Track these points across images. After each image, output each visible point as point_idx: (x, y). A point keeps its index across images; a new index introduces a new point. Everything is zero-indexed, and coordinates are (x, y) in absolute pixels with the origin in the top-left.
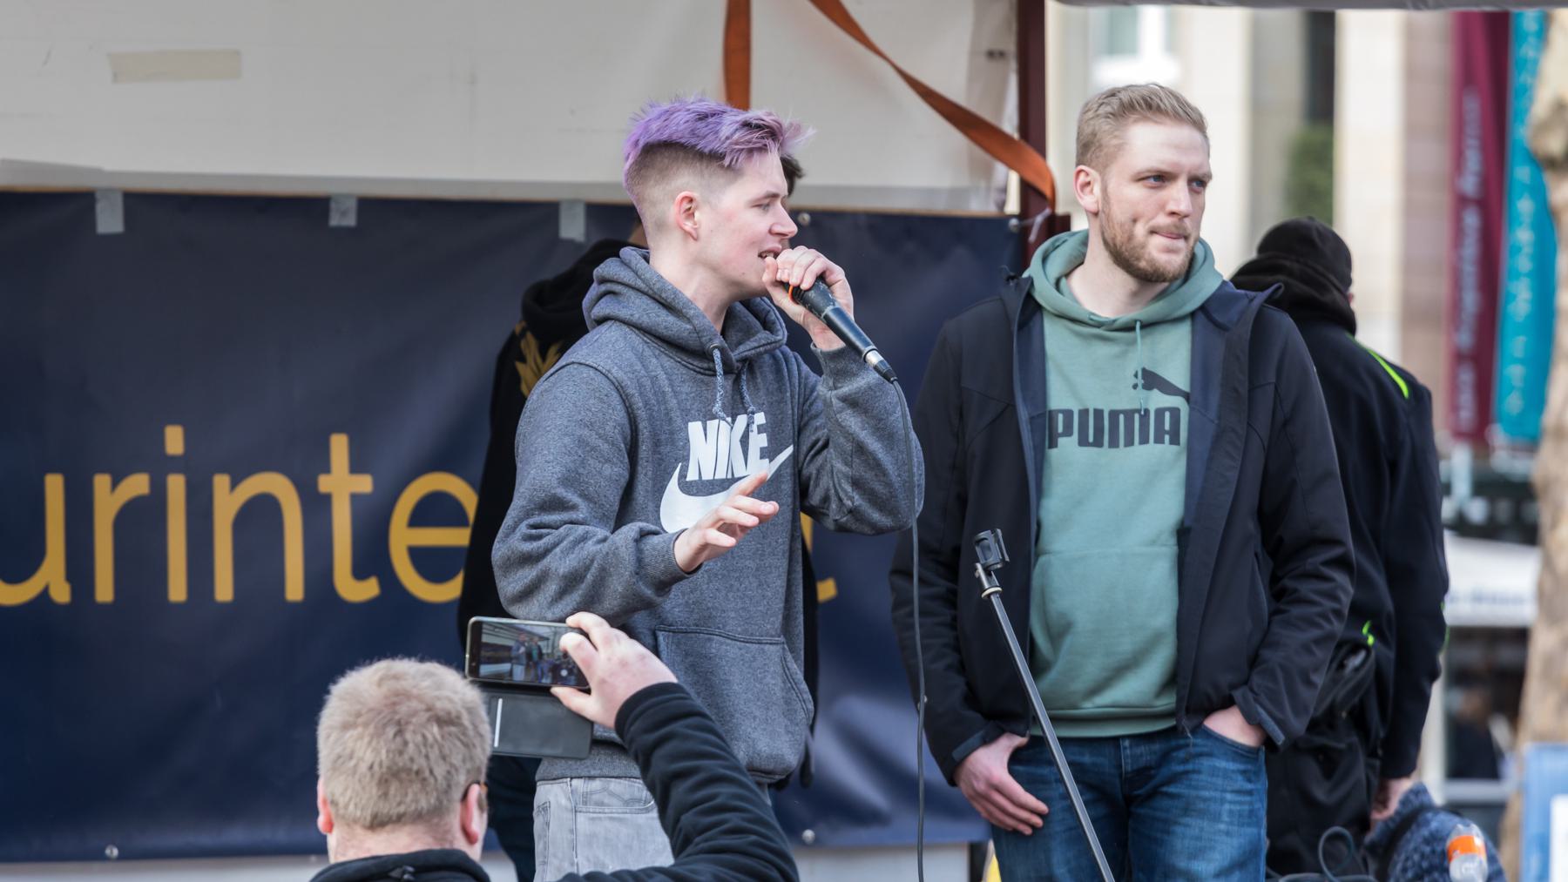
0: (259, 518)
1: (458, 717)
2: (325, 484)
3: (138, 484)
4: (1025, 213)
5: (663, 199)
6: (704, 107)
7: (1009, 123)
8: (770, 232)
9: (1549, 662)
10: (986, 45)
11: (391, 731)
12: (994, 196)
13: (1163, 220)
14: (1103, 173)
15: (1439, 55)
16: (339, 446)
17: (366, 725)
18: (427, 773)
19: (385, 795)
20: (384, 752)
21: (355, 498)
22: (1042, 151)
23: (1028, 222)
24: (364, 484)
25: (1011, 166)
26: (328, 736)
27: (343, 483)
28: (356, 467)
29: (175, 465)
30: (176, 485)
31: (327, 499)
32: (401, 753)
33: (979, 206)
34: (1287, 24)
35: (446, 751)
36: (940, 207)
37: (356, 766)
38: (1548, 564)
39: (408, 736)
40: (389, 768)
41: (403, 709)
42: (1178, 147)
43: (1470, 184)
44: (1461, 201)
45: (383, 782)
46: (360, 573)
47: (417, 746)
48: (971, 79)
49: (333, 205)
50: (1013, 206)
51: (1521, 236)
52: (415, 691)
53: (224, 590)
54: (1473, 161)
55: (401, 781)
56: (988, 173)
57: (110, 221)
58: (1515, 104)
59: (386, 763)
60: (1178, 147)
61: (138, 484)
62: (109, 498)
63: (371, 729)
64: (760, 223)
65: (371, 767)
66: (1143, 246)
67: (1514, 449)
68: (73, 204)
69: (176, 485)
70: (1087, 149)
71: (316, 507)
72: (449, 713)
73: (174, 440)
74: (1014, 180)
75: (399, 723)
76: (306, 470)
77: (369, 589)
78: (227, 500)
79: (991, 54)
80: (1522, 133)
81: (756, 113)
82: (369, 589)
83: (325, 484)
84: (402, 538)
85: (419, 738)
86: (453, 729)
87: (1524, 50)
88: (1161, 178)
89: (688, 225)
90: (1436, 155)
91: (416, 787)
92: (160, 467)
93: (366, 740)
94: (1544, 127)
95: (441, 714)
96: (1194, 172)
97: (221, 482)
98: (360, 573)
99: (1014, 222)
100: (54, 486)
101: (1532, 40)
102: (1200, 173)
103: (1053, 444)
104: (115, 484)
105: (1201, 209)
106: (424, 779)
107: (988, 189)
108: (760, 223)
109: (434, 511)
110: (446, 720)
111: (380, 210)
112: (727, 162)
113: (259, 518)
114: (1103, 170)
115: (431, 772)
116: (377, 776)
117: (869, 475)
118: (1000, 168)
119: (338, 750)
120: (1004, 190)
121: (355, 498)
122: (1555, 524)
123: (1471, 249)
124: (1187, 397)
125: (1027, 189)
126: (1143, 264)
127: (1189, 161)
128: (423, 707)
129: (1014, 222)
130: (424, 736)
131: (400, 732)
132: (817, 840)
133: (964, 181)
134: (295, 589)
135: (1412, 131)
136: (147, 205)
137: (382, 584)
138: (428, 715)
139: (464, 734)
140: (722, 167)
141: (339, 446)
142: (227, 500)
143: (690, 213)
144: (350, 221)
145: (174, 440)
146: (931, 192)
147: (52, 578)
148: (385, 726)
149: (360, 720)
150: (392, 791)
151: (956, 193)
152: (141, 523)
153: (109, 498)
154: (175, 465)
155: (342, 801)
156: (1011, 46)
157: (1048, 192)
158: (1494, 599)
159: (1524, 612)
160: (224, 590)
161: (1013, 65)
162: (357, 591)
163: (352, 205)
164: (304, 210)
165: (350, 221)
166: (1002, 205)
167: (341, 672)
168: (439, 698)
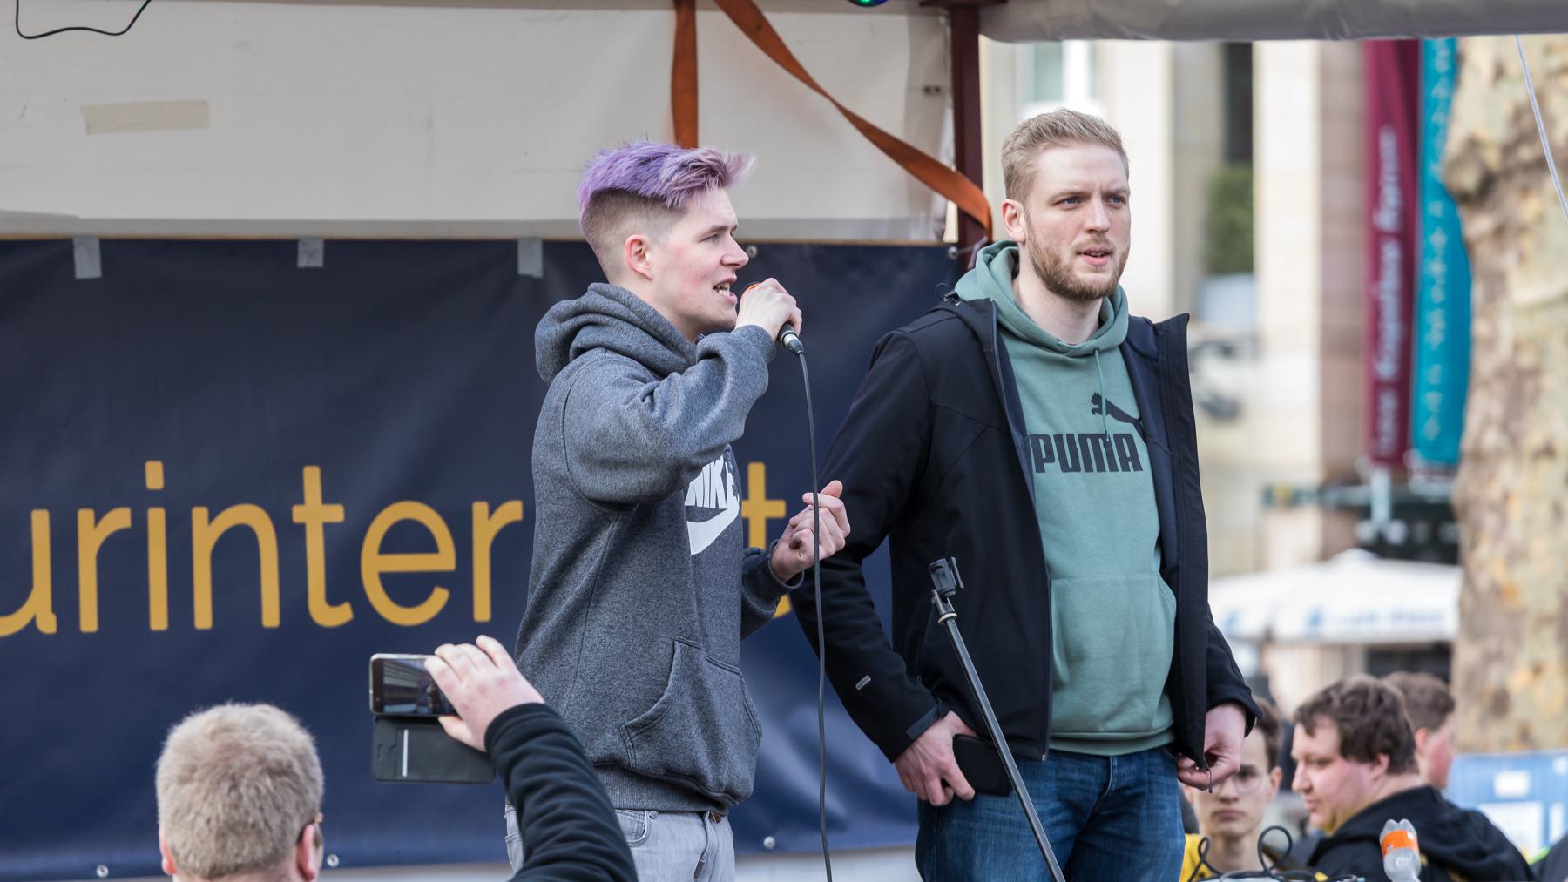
0: (236, 551)
1: (290, 766)
2: (299, 514)
3: (120, 518)
4: (963, 241)
5: (617, 243)
6: (646, 151)
7: (946, 155)
8: (722, 263)
9: (1471, 676)
10: (921, 82)
11: (226, 786)
12: (933, 226)
13: (1083, 239)
14: (1024, 202)
15: (1352, 96)
16: (312, 477)
17: (201, 780)
18: (262, 825)
19: (224, 847)
20: (220, 807)
21: (328, 528)
22: (978, 181)
23: (967, 250)
24: (336, 513)
25: (948, 197)
26: (166, 788)
27: (316, 513)
28: (328, 498)
29: (156, 498)
30: (157, 519)
31: (301, 528)
32: (236, 807)
33: (919, 235)
34: (1204, 56)
35: (280, 801)
36: (882, 237)
37: (193, 821)
38: (1468, 582)
39: (242, 789)
40: (226, 822)
41: (236, 764)
42: (1088, 167)
43: (1387, 219)
44: (1377, 238)
45: (221, 836)
46: (333, 599)
47: (251, 800)
48: (908, 115)
49: (301, 247)
50: (951, 235)
51: (1434, 268)
52: (247, 745)
53: (203, 618)
54: (1391, 196)
55: (237, 834)
56: (927, 204)
57: (87, 267)
58: (1428, 142)
59: (222, 817)
60: (1088, 167)
61: (120, 518)
62: (92, 533)
63: (207, 784)
64: (709, 256)
65: (208, 821)
66: (1069, 269)
67: (1431, 473)
68: (52, 252)
70: (1015, 182)
71: (291, 537)
72: (280, 763)
73: (154, 476)
74: (952, 210)
75: (233, 777)
76: (281, 501)
77: (341, 615)
78: (206, 532)
79: (927, 90)
80: (1435, 170)
81: (700, 154)
82: (341, 615)
83: (299, 514)
84: (374, 564)
85: (252, 792)
86: (286, 779)
87: (1435, 91)
88: (1076, 199)
89: (641, 267)
90: (1350, 192)
91: (253, 838)
92: (140, 501)
93: (203, 794)
94: (1457, 164)
95: (273, 765)
96: (1105, 188)
97: (199, 514)
98: (333, 599)
99: (953, 250)
100: (40, 521)
101: (1444, 80)
102: (1114, 187)
103: (1041, 469)
104: (98, 519)
105: (1125, 231)
106: (260, 832)
107: (928, 219)
108: (709, 256)
109: (407, 538)
110: (278, 771)
111: (351, 253)
112: (669, 202)
113: (236, 551)
114: (1024, 199)
115: (266, 823)
116: (214, 831)
118: (939, 199)
119: (176, 804)
120: (943, 220)
121: (328, 528)
122: (1474, 544)
123: (1390, 282)
124: (1136, 423)
125: (965, 218)
126: (1070, 286)
127: (1103, 178)
128: (255, 759)
129: (953, 250)
130: (257, 789)
131: (234, 787)
132: (777, 845)
133: (904, 212)
134: (271, 616)
135: (1327, 170)
136: (122, 251)
137: (355, 610)
138: (259, 768)
139: (297, 783)
140: (665, 207)
141: (312, 477)
142: (206, 532)
143: (641, 255)
144: (318, 262)
145: (154, 476)
146: (874, 223)
147: (39, 610)
148: (219, 782)
149: (196, 775)
150: (229, 844)
151: (895, 223)
152: (123, 555)
153: (92, 533)
154: (156, 498)
155: (182, 852)
156: (946, 82)
157: (985, 222)
158: (1413, 617)
159: (1447, 626)
160: (203, 618)
161: (949, 100)
162: (330, 616)
163: (320, 246)
164: (275, 252)
165: (318, 262)
166: (941, 234)
167: (178, 719)
168: (270, 749)
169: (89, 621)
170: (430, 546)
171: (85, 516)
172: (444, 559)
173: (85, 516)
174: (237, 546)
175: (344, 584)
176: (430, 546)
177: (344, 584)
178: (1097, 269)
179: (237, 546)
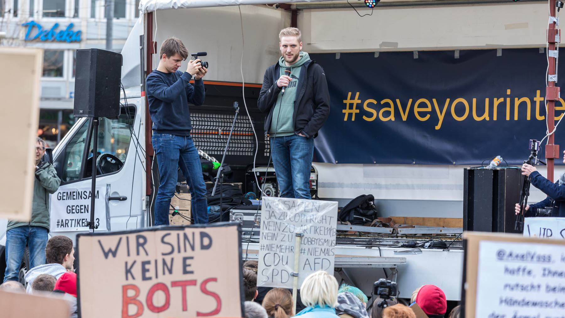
0: (523, 106)
2: (535, 99)
3: (502, 100)
21: (356, 114)
29: (508, 96)
30: (508, 100)
46: (541, 115)
53: (516, 118)
57: (499, 54)
61: (502, 100)
62: (496, 102)
68: (494, 51)
69: (508, 100)
71: (533, 103)
73: (509, 92)
78: (517, 102)
83: (535, 99)
92: (505, 96)
97: (516, 99)
98: (541, 115)
109: (423, 105)
111: (508, 52)
113: (523, 106)
117: (71, 202)
121: (356, 114)
134: (529, 118)
136: (505, 51)
142: (517, 102)
145: (509, 92)
152: (502, 106)
153: (496, 102)
154: (508, 96)
160: (516, 118)
162: (539, 118)
164: (492, 52)
169: (495, 118)
170: (427, 107)
171: (495, 99)
172: (429, 109)
173: (495, 99)
174: (523, 104)
175: (543, 112)
176: (427, 107)
177: (543, 112)
178: (289, 58)
179: (523, 104)
